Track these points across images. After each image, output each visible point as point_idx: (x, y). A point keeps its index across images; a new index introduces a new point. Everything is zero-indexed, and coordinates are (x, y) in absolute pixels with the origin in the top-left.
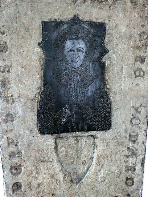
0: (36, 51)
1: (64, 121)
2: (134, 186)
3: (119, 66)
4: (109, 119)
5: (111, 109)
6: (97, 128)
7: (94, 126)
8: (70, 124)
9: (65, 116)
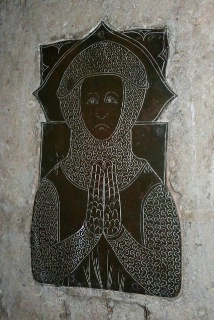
0: (28, 107)
2: (40, 45)
4: (175, 270)
6: (147, 288)
7: (139, 282)
8: (89, 269)
9: (79, 251)
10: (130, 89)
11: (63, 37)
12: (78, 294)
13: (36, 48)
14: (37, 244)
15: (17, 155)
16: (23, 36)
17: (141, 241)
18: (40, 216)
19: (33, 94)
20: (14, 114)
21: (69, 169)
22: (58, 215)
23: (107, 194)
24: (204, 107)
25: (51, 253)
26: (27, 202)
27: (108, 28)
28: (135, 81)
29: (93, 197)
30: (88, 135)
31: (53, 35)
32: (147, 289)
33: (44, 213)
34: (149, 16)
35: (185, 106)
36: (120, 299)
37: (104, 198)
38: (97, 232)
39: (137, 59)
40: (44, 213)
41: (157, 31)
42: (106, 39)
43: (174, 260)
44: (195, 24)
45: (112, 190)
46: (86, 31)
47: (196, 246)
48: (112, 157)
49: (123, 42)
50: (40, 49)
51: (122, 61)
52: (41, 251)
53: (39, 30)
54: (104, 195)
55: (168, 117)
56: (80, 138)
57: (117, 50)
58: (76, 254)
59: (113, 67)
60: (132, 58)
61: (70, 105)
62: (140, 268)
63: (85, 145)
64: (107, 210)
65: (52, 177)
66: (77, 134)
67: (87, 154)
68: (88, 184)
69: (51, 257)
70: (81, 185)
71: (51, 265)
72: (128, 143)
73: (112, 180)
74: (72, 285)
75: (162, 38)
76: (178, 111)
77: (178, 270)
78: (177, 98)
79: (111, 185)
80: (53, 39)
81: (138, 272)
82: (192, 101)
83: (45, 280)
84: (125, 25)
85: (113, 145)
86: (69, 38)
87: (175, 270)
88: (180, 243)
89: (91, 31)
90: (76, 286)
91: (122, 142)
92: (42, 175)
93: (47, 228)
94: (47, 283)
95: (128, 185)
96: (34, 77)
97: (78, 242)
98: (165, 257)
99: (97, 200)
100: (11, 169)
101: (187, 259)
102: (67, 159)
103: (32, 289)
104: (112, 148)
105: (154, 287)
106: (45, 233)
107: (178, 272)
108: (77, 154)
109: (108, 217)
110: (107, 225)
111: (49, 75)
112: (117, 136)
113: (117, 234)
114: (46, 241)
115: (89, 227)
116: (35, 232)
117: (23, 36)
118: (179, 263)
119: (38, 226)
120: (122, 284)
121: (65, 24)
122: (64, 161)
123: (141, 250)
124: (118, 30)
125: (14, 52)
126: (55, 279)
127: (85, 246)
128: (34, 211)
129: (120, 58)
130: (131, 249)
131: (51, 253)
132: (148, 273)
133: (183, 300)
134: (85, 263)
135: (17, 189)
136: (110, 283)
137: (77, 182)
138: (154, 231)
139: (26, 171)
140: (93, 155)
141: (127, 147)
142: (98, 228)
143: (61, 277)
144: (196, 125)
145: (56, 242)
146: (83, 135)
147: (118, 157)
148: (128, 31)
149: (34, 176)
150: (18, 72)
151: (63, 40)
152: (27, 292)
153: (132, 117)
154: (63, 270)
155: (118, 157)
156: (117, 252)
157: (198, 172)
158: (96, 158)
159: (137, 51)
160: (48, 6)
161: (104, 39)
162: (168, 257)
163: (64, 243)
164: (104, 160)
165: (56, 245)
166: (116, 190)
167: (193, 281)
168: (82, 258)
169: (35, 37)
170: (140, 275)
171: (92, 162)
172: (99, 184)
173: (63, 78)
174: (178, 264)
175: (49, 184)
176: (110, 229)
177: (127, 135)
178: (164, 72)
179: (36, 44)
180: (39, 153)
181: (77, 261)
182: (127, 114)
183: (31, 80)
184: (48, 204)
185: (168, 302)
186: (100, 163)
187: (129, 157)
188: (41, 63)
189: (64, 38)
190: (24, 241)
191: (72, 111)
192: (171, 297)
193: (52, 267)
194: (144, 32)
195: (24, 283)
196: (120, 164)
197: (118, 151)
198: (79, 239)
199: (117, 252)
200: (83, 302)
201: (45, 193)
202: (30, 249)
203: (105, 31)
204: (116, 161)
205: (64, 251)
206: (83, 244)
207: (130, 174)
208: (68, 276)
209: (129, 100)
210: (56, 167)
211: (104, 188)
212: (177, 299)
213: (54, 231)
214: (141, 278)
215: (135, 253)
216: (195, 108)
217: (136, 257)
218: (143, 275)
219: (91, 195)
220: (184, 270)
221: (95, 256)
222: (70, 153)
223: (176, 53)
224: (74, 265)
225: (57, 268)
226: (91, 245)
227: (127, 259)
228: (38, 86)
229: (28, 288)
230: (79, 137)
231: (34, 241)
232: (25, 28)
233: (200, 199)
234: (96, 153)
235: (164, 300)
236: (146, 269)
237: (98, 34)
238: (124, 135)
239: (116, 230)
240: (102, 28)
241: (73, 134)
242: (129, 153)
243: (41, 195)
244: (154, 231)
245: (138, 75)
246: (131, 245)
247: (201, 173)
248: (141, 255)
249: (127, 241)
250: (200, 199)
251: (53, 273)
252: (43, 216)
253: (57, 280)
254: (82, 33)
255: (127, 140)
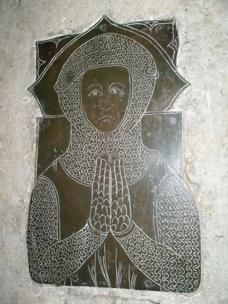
0: (23, 102)
1: (82, 261)
2: (35, 41)
3: (221, 121)
4: (194, 264)
5: (199, 238)
6: (162, 284)
7: (153, 278)
8: (94, 268)
9: (83, 250)
10: (138, 79)
11: (61, 32)
12: (81, 293)
13: (32, 44)
14: (34, 244)
15: (10, 152)
16: (18, 34)
17: (154, 236)
18: (37, 215)
19: (28, 89)
20: (7, 111)
21: (69, 165)
22: (57, 213)
23: (114, 189)
24: (220, 94)
25: (50, 253)
26: (22, 201)
27: (111, 22)
28: (143, 71)
29: (98, 193)
30: (90, 128)
31: (50, 31)
32: (163, 286)
33: (42, 212)
34: (155, 8)
35: (199, 94)
36: (130, 296)
37: (110, 194)
38: (104, 229)
39: (144, 50)
40: (42, 212)
41: (165, 22)
42: (109, 31)
43: (192, 254)
44: (206, 14)
45: (119, 185)
46: (86, 25)
47: (217, 238)
48: (120, 150)
49: (128, 34)
50: (36, 45)
51: (127, 52)
52: (39, 250)
53: (34, 27)
54: (110, 190)
55: (181, 107)
56: (81, 131)
57: (121, 42)
58: (79, 254)
59: (118, 58)
60: (140, 50)
61: (69, 99)
62: (153, 265)
63: (87, 138)
64: (114, 207)
65: (50, 174)
66: (78, 128)
67: (90, 148)
68: (92, 180)
69: (51, 257)
70: (84, 181)
71: (50, 265)
72: (138, 134)
73: (119, 175)
74: (75, 285)
75: (171, 30)
76: (192, 100)
77: (197, 264)
78: (190, 87)
79: (119, 179)
80: (49, 35)
81: (152, 268)
82: (207, 89)
83: (44, 280)
84: (130, 17)
85: (119, 137)
86: (66, 32)
87: (194, 264)
88: (199, 236)
89: (92, 26)
90: (80, 285)
91: (130, 133)
92: (39, 172)
93: (45, 227)
94: (47, 283)
95: (139, 178)
96: (29, 73)
97: (82, 241)
98: (183, 251)
99: (102, 196)
100: (4, 167)
101: (207, 252)
102: (67, 154)
103: (30, 289)
104: (119, 140)
105: (170, 283)
106: (43, 232)
107: (197, 267)
108: (79, 149)
109: (116, 213)
110: (115, 221)
111: (46, 70)
112: (124, 128)
113: (127, 230)
114: (45, 241)
115: (93, 225)
116: (32, 232)
117: (18, 34)
118: (198, 257)
119: (35, 225)
120: (133, 282)
121: (63, 20)
122: (64, 157)
123: (155, 246)
124: (121, 23)
125: (7, 50)
126: (56, 279)
127: (90, 245)
128: (30, 210)
129: (126, 49)
130: (143, 245)
131: (50, 253)
132: (163, 269)
133: (203, 295)
134: (89, 262)
135: (11, 188)
136: (119, 281)
137: (79, 178)
138: (169, 225)
139: (20, 169)
140: (97, 149)
141: (136, 138)
142: (105, 226)
143: (63, 277)
144: (212, 113)
145: (56, 241)
146: (85, 128)
147: (126, 150)
148: (134, 23)
149: (30, 174)
150: (11, 69)
151: (61, 35)
152: (25, 293)
153: (141, 107)
154: (64, 270)
155: (126, 150)
156: (127, 250)
157: (217, 162)
158: (100, 152)
159: (143, 42)
160: (45, 4)
161: (106, 32)
162: (186, 251)
163: (65, 242)
164: (110, 153)
165: (56, 245)
166: (125, 184)
167: (214, 275)
168: (87, 257)
169: (30, 35)
170: (153, 271)
171: (96, 156)
172: (104, 179)
173: (62, 71)
174: (198, 258)
175: (46, 181)
176: (119, 226)
177: (136, 126)
178: (175, 62)
179: (32, 41)
180: (35, 150)
181: (81, 261)
182: (135, 104)
183: (26, 76)
184: (46, 203)
185: (186, 298)
186: (105, 157)
187: (139, 149)
188: (37, 59)
189: (62, 33)
190: (19, 241)
191: (72, 104)
192: (189, 292)
193: (52, 267)
194: (151, 23)
195: (20, 284)
196: (129, 157)
197: (126, 144)
198: (82, 237)
199: (127, 250)
200: (87, 301)
201: (42, 191)
202: (27, 249)
203: (108, 24)
204: (124, 153)
205: (65, 251)
206: (87, 243)
207: (141, 166)
208: (71, 276)
209: (137, 90)
210: (54, 164)
211: (110, 176)
212: (197, 293)
213: (53, 230)
214: (155, 275)
215: (148, 249)
216: (211, 96)
217: (149, 254)
218: (157, 272)
219: (96, 192)
220: (204, 263)
221: (102, 254)
222: (70, 147)
223: (187, 42)
224: (77, 264)
225: (58, 268)
226: (97, 243)
227: (138, 256)
228: (34, 80)
229: (25, 289)
230: (80, 130)
231: (31, 240)
232: (19, 27)
233: (220, 189)
234: (101, 146)
235: (181, 296)
236: (161, 265)
237: (100, 27)
238: (132, 126)
239: (125, 227)
240: (105, 22)
241: (73, 128)
242: (139, 144)
243: (37, 193)
244: (169, 225)
245: (146, 65)
246: (143, 241)
247: (221, 162)
248: (155, 251)
249: (138, 237)
250: (220, 189)
251: (53, 273)
252: (41, 215)
253: (59, 280)
254: (82, 28)
255: (136, 131)
